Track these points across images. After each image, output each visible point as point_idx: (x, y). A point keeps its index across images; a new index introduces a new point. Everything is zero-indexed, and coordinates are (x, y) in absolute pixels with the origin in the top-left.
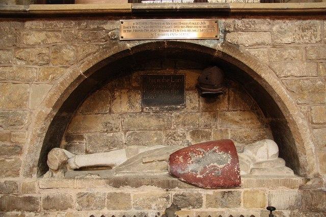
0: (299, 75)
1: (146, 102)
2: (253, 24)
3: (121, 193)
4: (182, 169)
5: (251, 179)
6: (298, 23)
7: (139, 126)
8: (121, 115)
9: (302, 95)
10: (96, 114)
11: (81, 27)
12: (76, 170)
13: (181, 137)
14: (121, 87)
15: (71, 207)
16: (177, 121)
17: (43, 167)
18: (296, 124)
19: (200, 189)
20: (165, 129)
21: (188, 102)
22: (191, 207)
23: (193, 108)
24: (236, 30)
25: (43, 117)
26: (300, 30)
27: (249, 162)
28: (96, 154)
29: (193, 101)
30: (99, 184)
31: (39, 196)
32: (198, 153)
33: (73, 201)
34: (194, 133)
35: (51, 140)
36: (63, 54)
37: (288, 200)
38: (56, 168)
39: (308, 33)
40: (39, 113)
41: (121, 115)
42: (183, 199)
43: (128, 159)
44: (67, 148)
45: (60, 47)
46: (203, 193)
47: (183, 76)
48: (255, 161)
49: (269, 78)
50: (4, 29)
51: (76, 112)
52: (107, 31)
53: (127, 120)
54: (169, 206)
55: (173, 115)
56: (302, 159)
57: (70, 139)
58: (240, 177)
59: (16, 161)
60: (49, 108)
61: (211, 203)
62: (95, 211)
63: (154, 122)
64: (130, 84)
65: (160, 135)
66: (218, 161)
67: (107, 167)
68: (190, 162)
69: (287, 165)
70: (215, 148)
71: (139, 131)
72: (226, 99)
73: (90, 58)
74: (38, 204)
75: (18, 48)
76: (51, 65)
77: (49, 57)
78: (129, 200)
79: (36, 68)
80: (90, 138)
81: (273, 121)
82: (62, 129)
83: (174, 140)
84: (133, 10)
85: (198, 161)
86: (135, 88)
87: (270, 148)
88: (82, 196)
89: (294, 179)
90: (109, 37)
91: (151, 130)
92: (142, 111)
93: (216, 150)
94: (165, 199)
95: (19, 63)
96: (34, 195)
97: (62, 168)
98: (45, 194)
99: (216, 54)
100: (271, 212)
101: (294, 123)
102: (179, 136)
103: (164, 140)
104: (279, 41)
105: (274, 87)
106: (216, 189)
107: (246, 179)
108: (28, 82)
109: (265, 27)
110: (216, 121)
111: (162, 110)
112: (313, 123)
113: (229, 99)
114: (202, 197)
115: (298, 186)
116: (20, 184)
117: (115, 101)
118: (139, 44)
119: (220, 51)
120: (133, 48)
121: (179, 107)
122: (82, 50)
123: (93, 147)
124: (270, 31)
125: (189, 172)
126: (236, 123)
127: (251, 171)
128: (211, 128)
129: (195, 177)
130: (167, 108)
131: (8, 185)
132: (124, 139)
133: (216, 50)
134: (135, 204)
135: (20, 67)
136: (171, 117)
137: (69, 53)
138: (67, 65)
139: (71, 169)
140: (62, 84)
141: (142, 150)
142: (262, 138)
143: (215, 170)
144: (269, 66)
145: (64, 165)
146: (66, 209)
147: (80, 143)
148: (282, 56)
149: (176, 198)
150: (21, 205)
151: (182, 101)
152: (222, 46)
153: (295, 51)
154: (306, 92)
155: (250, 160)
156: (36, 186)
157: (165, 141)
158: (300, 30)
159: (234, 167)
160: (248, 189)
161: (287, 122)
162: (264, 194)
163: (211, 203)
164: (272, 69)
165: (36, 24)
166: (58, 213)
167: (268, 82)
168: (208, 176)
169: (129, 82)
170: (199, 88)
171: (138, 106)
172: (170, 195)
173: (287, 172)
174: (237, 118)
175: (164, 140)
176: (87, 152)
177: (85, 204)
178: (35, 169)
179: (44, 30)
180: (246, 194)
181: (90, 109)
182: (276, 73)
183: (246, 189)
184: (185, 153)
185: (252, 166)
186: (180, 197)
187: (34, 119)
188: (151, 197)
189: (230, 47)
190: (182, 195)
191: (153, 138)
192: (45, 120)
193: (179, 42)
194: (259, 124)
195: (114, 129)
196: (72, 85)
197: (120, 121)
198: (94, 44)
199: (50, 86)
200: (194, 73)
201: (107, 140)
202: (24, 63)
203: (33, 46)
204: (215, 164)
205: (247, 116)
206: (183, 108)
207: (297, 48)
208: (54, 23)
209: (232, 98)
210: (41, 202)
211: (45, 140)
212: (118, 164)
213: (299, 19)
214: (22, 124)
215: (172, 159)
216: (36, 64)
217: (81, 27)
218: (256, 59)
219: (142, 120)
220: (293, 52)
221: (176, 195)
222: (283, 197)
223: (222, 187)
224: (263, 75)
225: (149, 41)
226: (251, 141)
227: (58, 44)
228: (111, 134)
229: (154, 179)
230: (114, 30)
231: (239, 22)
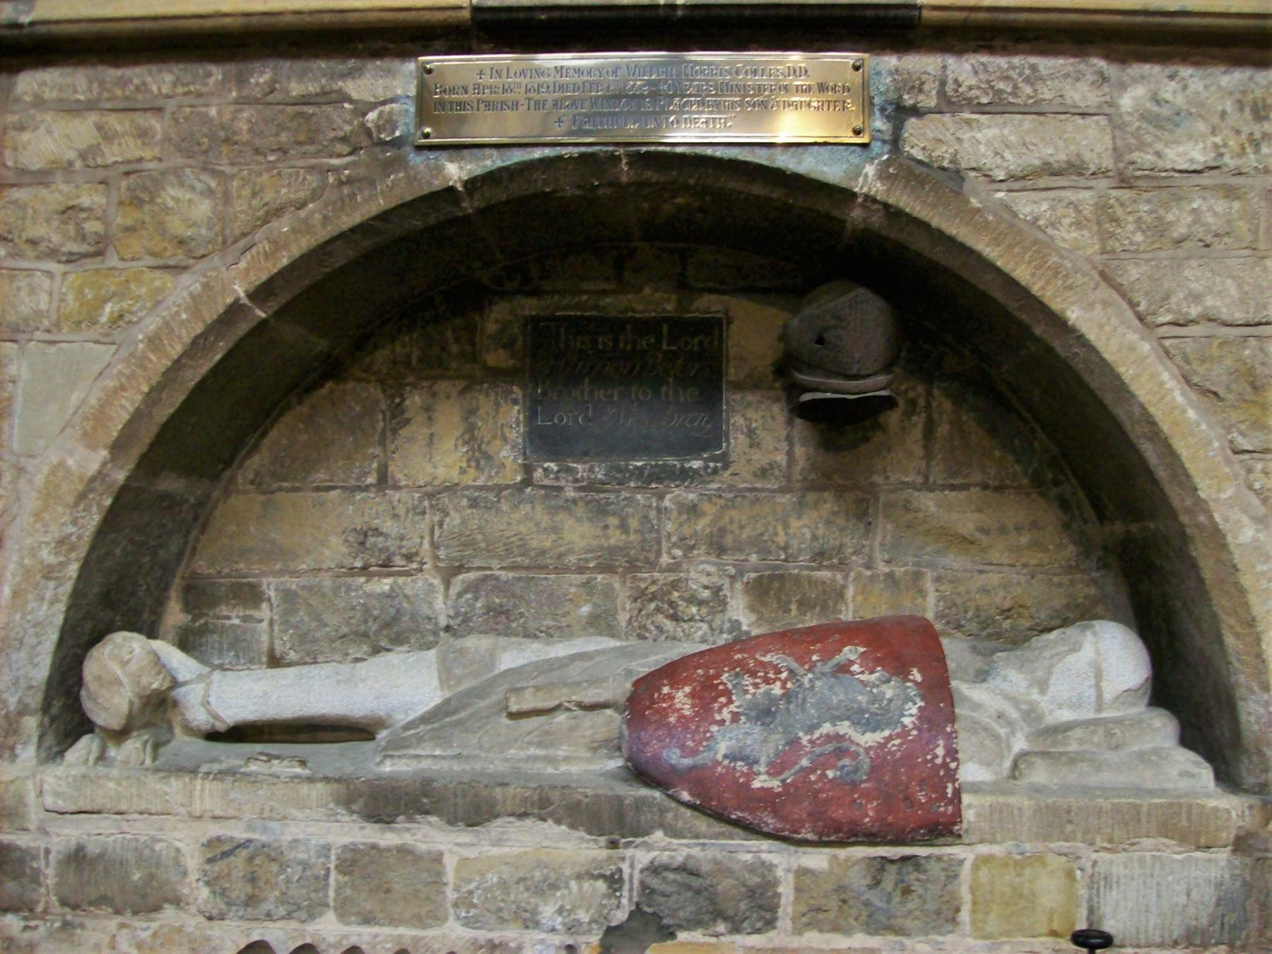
0: (1239, 316)
2: (1027, 80)
3: (403, 851)
4: (683, 747)
5: (1012, 800)
6: (1233, 78)
7: (509, 551)
8: (430, 496)
9: (1256, 411)
10: (318, 489)
11: (246, 92)
12: (213, 736)
13: (701, 603)
14: (432, 368)
15: (177, 901)
16: (686, 531)
17: (66, 715)
18: (1224, 547)
19: (765, 844)
20: (632, 567)
21: (737, 442)
22: (721, 927)
23: (763, 473)
25: (69, 491)
26: (1241, 109)
27: (1010, 723)
28: (313, 670)
29: (761, 435)
30: (302, 805)
31: (41, 843)
32: (765, 673)
33: (185, 874)
34: (765, 590)
35: (109, 599)
36: (166, 209)
37: (1182, 899)
38: (116, 723)
40: (54, 470)
41: (430, 496)
42: (689, 887)
43: (448, 694)
44: (186, 643)
45: (156, 181)
46: (783, 861)
48: (1040, 717)
49: (1097, 321)
51: (232, 479)
52: (362, 109)
53: (457, 521)
54: (620, 916)
55: (667, 503)
57: (199, 597)
58: (957, 793)
60: (92, 447)
61: (819, 910)
62: (280, 924)
63: (578, 534)
64: (474, 357)
65: (608, 593)
66: (861, 712)
67: (353, 731)
68: (726, 714)
69: (1186, 741)
70: (850, 653)
71: (511, 575)
72: (917, 432)
73: (283, 226)
74: (36, 878)
76: (113, 260)
78: (437, 881)
79: (50, 274)
80: (289, 597)
81: (1125, 537)
82: (155, 545)
83: (675, 618)
85: (764, 714)
86: (497, 376)
87: (1110, 659)
88: (225, 855)
89: (1212, 803)
90: (369, 133)
91: (567, 569)
93: (852, 662)
94: (601, 886)
96: (22, 840)
97: (146, 725)
98: (67, 835)
99: (856, 214)
101: (1217, 537)
102: (692, 600)
103: (623, 618)
104: (1147, 158)
105: (1126, 372)
106: (842, 844)
107: (988, 800)
109: (1082, 94)
110: (867, 532)
111: (620, 478)
114: (776, 883)
115: (1228, 835)
117: (404, 433)
118: (499, 164)
119: (874, 201)
120: (473, 184)
121: (696, 464)
122: (246, 192)
123: (303, 638)
124: (1108, 113)
126: (965, 543)
127: (1015, 766)
128: (843, 565)
129: (747, 785)
130: (640, 470)
132: (441, 608)
133: (854, 195)
134: (464, 901)
136: (659, 510)
137: (190, 206)
138: (180, 258)
139: (190, 730)
140: (154, 342)
141: (514, 656)
142: (1077, 614)
143: (840, 753)
144: (1103, 274)
145: (158, 708)
146: (157, 909)
147: (245, 619)
148: (1159, 229)
149: (655, 882)
151: (709, 441)
152: (882, 175)
153: (1221, 206)
155: (1014, 714)
156: (31, 797)
157: (630, 622)
158: (1241, 109)
159: (932, 742)
160: (997, 850)
161: (1184, 538)
162: (1070, 875)
163: (819, 910)
164: (1118, 288)
165: (59, 80)
166: (122, 926)
167: (1100, 345)
168: (807, 782)
169: (468, 348)
170: (786, 374)
171: (508, 456)
172: (625, 867)
173: (1184, 774)
174: (967, 523)
175: (623, 618)
176: (275, 661)
177: (240, 890)
178: (31, 723)
180: (984, 874)
181: (291, 472)
182: (1133, 305)
183: (983, 849)
184: (703, 676)
185: (1020, 744)
186: (671, 876)
188: (537, 874)
189: (922, 181)
190: (682, 869)
191: (578, 606)
192: (76, 504)
193: (682, 155)
194: (1070, 551)
195: (398, 560)
196: (196, 347)
197: (424, 526)
198: (301, 163)
200: (774, 310)
201: (367, 610)
203: (42, 178)
204: (844, 728)
205: (1014, 511)
206: (715, 471)
207: (1230, 193)
208: (137, 74)
209: (943, 429)
210: (50, 871)
211: (77, 594)
212: (402, 718)
213: (1239, 62)
215: (642, 701)
216: (53, 254)
217: (246, 92)
218: (1040, 235)
219: (523, 522)
220: (1214, 211)
221: (655, 869)
222: (1161, 887)
223: (872, 839)
224: (1074, 315)
225: (548, 152)
226: (1007, 633)
228: (385, 585)
229: (554, 787)
230: (392, 101)
231: (964, 69)
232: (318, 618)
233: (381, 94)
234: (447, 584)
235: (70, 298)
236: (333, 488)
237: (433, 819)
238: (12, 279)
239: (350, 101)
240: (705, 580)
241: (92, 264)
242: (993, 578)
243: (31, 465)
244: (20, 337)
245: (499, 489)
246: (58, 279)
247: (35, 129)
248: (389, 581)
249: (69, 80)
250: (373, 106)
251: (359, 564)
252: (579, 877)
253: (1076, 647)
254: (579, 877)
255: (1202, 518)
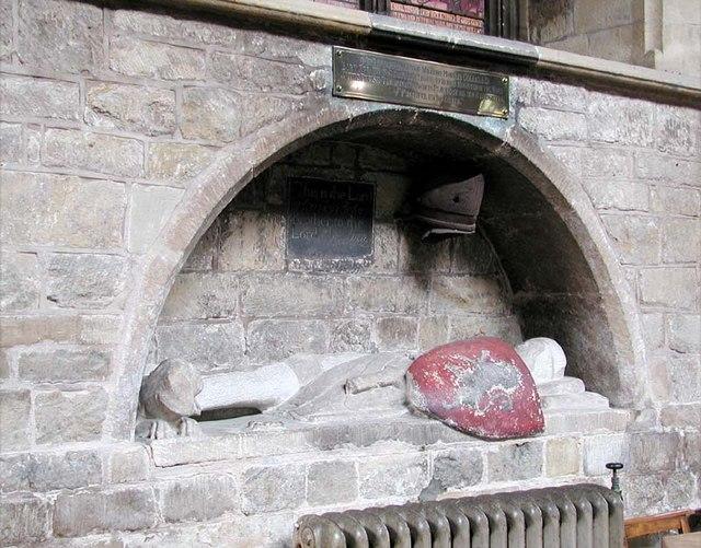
0: (624, 207)
1: (297, 248)
3: (338, 463)
6: (624, 102)
15: (231, 509)
20: (332, 316)
21: (377, 250)
23: (387, 266)
24: (535, 103)
29: (388, 247)
39: (636, 124)
40: (154, 264)
47: (372, 186)
50: (60, 22)
56: (625, 373)
59: (94, 396)
63: (309, 297)
64: (263, 199)
65: (321, 330)
73: (271, 129)
75: (95, 79)
76: (178, 138)
77: (176, 117)
83: (348, 342)
84: (374, 29)
85: (471, 382)
92: (287, 270)
94: (419, 469)
95: (98, 121)
96: (140, 487)
98: (167, 481)
99: (498, 150)
100: (615, 471)
108: (123, 178)
109: (577, 104)
112: (642, 302)
113: (451, 247)
116: (105, 459)
121: (360, 261)
125: (461, 406)
131: (75, 463)
134: (365, 485)
135: (101, 135)
137: (223, 110)
140: (207, 189)
149: (438, 465)
150: (109, 515)
151: (365, 250)
152: (512, 134)
153: (619, 158)
154: (633, 241)
166: (202, 527)
172: (428, 458)
179: (162, 41)
183: (549, 437)
187: (141, 281)
195: (223, 314)
197: (236, 294)
199: (180, 194)
201: (207, 343)
202: (110, 124)
203: (135, 81)
204: (500, 387)
207: (622, 153)
214: (110, 293)
216: (143, 130)
221: (438, 459)
224: (573, 203)
227: (194, 83)
228: (214, 329)
232: (181, 349)
233: (316, 64)
234: (246, 327)
235: (155, 158)
236: (192, 271)
237: (350, 445)
238: (121, 143)
239: (302, 64)
240: (361, 322)
241: (167, 139)
242: (473, 319)
243: (139, 260)
244: (126, 179)
245: (274, 273)
246: (147, 146)
247: (131, 49)
248: (217, 326)
249: (149, 21)
250: (314, 69)
251: (204, 317)
252: (410, 466)
253: (541, 350)
254: (410, 466)
255: (611, 292)
